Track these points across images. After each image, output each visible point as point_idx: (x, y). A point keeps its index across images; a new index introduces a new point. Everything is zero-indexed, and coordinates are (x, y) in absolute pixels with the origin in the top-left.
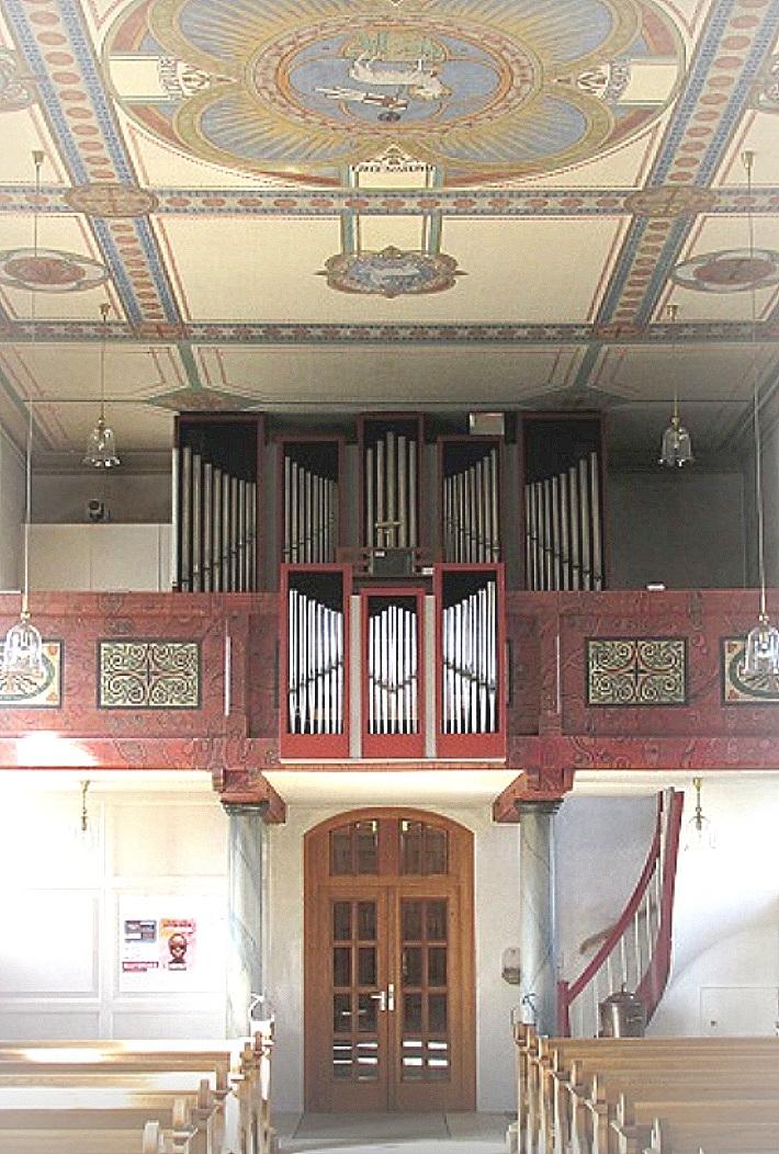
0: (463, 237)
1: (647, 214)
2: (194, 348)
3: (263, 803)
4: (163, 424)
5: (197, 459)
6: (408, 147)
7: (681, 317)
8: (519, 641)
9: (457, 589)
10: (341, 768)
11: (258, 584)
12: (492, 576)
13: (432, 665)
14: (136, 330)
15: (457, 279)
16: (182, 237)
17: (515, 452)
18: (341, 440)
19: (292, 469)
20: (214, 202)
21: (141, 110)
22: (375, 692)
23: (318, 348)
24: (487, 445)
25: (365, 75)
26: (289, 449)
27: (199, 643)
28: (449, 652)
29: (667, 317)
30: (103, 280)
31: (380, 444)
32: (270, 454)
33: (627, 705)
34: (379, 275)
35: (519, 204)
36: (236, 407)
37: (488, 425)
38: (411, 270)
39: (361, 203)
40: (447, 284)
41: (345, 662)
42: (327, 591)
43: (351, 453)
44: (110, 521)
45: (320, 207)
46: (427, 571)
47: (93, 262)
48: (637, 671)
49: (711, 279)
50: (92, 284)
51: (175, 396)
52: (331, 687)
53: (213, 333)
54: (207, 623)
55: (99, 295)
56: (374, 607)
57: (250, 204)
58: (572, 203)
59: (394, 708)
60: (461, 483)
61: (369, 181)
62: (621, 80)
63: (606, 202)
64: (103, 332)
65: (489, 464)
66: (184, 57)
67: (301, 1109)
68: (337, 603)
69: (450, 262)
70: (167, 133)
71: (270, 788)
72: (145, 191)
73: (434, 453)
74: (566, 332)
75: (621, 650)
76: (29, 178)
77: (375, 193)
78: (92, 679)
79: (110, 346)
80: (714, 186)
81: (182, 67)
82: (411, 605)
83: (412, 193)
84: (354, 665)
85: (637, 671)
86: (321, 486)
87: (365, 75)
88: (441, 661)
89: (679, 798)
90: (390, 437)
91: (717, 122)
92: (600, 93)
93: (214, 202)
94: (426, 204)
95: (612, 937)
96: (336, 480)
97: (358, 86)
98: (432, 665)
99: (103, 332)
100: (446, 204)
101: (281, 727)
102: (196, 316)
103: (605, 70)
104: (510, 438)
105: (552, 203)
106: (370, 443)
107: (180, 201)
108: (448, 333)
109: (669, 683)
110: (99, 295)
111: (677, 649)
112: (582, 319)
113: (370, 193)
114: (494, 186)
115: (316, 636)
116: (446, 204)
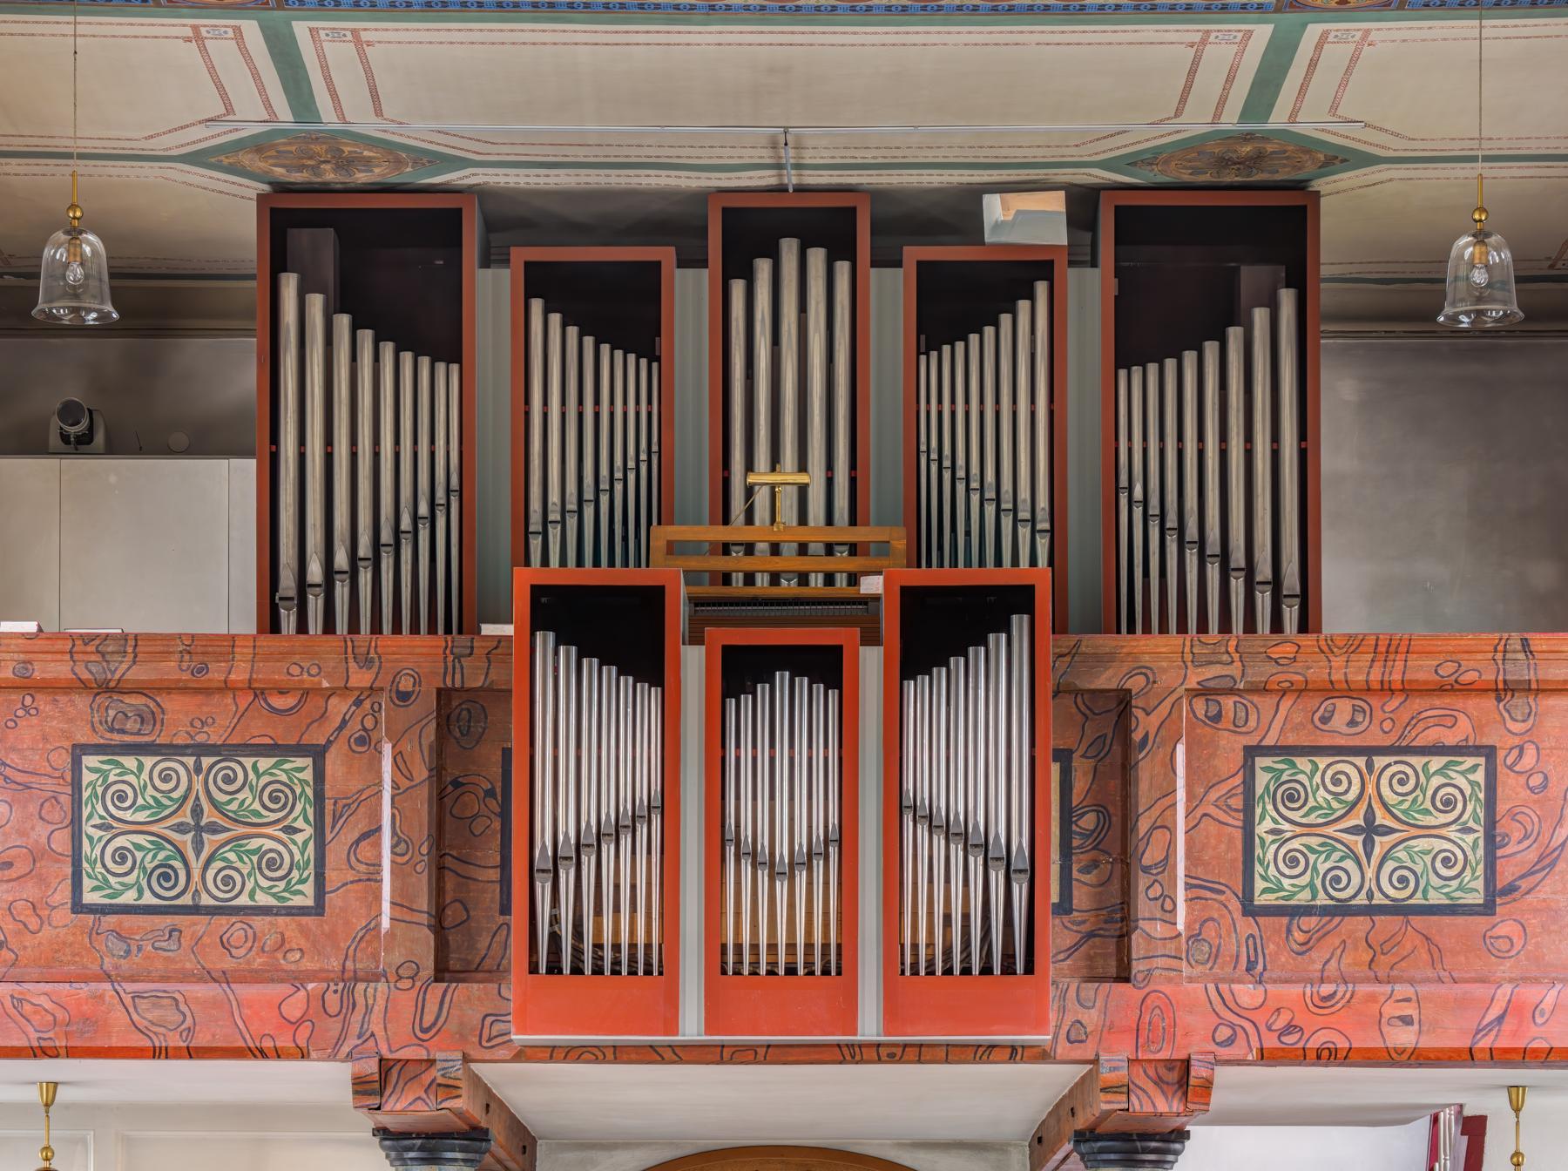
3: (474, 1136)
5: (316, 302)
8: (1096, 749)
17: (1089, 294)
18: (665, 255)
19: (552, 333)
24: (1020, 275)
27: (318, 754)
28: (922, 781)
31: (763, 267)
32: (491, 293)
33: (1343, 910)
36: (408, 175)
37: (1022, 220)
43: (689, 294)
46: (872, 585)
51: (258, 145)
52: (629, 867)
71: (491, 1102)
73: (892, 294)
75: (1326, 782)
78: (61, 841)
82: (826, 667)
85: (1370, 830)
86: (620, 370)
89: (1474, 1128)
90: (789, 248)
106: (737, 266)
109: (1437, 856)
111: (1468, 776)
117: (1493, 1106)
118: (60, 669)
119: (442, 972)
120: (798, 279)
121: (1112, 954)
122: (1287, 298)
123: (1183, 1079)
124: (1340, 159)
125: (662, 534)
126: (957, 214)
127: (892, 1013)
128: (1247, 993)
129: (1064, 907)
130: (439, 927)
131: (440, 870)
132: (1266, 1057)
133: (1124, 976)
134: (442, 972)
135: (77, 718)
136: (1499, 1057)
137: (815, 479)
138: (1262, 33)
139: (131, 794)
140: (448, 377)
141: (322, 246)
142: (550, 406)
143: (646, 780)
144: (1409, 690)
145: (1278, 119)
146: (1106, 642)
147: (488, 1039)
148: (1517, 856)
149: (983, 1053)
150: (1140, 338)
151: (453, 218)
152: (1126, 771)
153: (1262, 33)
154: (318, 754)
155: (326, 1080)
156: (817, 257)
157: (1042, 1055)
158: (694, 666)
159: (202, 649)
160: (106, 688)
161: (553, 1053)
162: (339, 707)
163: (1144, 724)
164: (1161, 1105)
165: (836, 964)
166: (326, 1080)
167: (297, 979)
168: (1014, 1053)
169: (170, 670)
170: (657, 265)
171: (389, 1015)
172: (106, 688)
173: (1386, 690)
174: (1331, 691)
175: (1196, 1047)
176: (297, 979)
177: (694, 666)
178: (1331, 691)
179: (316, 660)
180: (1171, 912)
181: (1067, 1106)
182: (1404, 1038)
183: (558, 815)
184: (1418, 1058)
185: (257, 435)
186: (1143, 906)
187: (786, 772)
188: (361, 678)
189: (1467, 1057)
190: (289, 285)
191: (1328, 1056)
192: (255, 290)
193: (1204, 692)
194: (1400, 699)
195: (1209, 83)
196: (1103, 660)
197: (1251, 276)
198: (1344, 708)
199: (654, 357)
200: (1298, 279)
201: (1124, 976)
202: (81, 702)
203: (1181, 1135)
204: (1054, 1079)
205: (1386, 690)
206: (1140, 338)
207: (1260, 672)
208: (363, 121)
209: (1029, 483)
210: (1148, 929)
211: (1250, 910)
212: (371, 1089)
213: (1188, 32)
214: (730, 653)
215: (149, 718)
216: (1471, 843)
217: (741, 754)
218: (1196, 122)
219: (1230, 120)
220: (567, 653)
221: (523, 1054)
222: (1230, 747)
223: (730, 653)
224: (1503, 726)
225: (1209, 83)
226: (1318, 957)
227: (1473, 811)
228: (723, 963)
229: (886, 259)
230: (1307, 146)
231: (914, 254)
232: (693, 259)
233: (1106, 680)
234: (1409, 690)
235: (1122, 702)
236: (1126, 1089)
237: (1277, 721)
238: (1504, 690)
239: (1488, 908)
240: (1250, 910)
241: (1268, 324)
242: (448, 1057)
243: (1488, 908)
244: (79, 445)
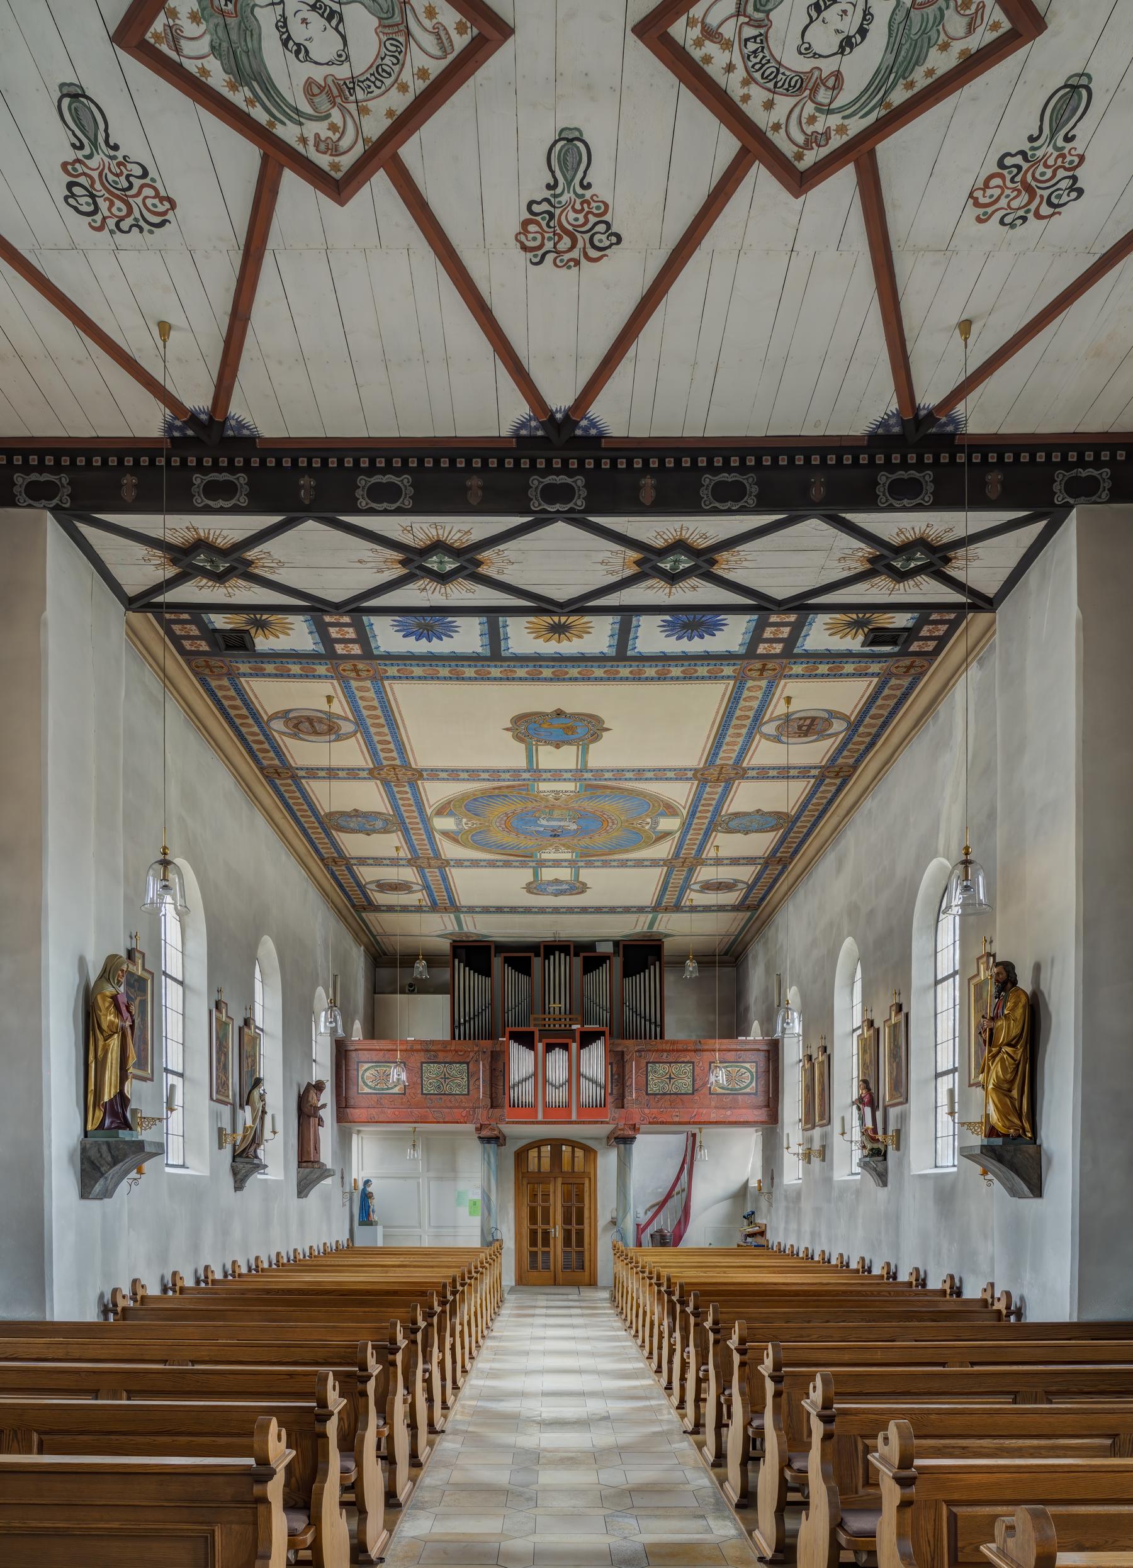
0: (586, 875)
1: (674, 866)
2: (462, 916)
3: (497, 1138)
4: (445, 945)
5: (462, 965)
6: (564, 845)
7: (695, 903)
8: (617, 1063)
9: (587, 1039)
10: (533, 1123)
11: (491, 1036)
12: (603, 1033)
13: (575, 1073)
14: (434, 908)
15: (605, 734)
16: (459, 878)
17: (618, 962)
18: (532, 955)
19: (509, 971)
20: (475, 863)
21: (446, 834)
22: (549, 1088)
23: (522, 916)
24: (602, 959)
25: (544, 822)
26: (507, 960)
27: (468, 1064)
28: (583, 1070)
29: (688, 903)
30: (355, 733)
31: (552, 957)
32: (497, 962)
33: (665, 1094)
34: (550, 889)
35: (615, 864)
36: (480, 939)
37: (606, 948)
38: (565, 887)
39: (542, 864)
40: (582, 892)
41: (535, 1074)
42: (526, 1040)
43: (537, 962)
44: (419, 992)
45: (523, 865)
46: (574, 1027)
47: (346, 719)
48: (670, 1078)
49: (708, 889)
50: (416, 891)
51: (451, 934)
52: (529, 1086)
53: (471, 910)
54: (472, 1054)
55: (419, 895)
56: (549, 1048)
57: (492, 864)
58: (639, 863)
59: (557, 1096)
60: (594, 975)
61: (545, 856)
62: (657, 823)
63: (654, 863)
64: (419, 909)
65: (606, 967)
66: (466, 816)
67: (513, 1284)
68: (531, 1046)
69: (584, 884)
70: (456, 841)
71: (500, 1132)
72: (415, 770)
73: (578, 962)
74: (641, 910)
75: (662, 1069)
76: (394, 854)
77: (549, 860)
78: (419, 1081)
79: (423, 915)
80: (745, 765)
81: (464, 820)
82: (565, 1047)
83: (566, 861)
84: (539, 1075)
85: (670, 1078)
86: (524, 979)
87: (544, 822)
88: (579, 1075)
89: (694, 1135)
90: (557, 953)
91: (749, 721)
92: (647, 827)
93: (475, 863)
94: (572, 864)
95: (662, 1204)
96: (530, 975)
97: (541, 826)
98: (575, 1073)
99: (419, 909)
100: (581, 864)
101: (507, 1104)
102: (463, 904)
103: (649, 820)
104: (616, 952)
105: (629, 863)
106: (547, 957)
107: (459, 863)
108: (584, 910)
109: (684, 1083)
110: (419, 895)
111: (689, 1067)
112: (648, 904)
113: (545, 860)
114: (603, 858)
115: (521, 1062)
116: (581, 864)
117: (696, 1131)
118: (419, 1047)
119: (492, 1107)
120: (559, 958)
121: (620, 1102)
122: (657, 963)
123: (635, 1128)
124: (667, 936)
125: (532, 1017)
126: (590, 946)
127: (579, 1114)
128: (647, 1111)
129: (611, 1094)
130: (491, 1098)
131: (491, 1087)
132: (650, 1123)
133: (623, 1107)
134: (492, 1107)
135: (421, 1057)
136: (695, 1123)
137: (562, 1005)
138: (650, 916)
139: (432, 1071)
140: (488, 980)
141: (463, 953)
142: (509, 988)
143: (531, 1069)
144: (678, 1051)
145: (655, 929)
146: (620, 1041)
147: (501, 1120)
148: (698, 1083)
149: (596, 1123)
150: (628, 972)
151: (489, 947)
152: (623, 1066)
153: (650, 916)
154: (468, 1064)
155: (470, 1127)
156: (563, 955)
157: (607, 1123)
158: (540, 1046)
159: (444, 1042)
160: (427, 1051)
161: (513, 1123)
162: (472, 1054)
163: (627, 1058)
164: (631, 1133)
165: (568, 1106)
166: (470, 1127)
167: (465, 1108)
168: (602, 1122)
169: (440, 1047)
170: (530, 957)
171: (482, 1115)
172: (427, 1051)
173: (673, 1051)
174: (663, 1051)
175: (637, 1121)
176: (465, 1108)
177: (540, 1046)
178: (663, 1051)
179: (468, 1045)
180: (632, 1095)
181: (613, 1132)
182: (677, 1119)
183: (515, 1076)
184: (679, 1123)
185: (447, 988)
186: (627, 1094)
187: (557, 1065)
188: (476, 1049)
189: (689, 1123)
190: (456, 961)
191: (662, 1123)
192: (450, 958)
193: (638, 1051)
194: (678, 1051)
195: (640, 924)
196: (618, 1045)
197: (650, 959)
198: (665, 1054)
199: (530, 975)
200: (659, 960)
201: (623, 1107)
202: (422, 1053)
203: (633, 1139)
204: (610, 1127)
205: (673, 1051)
206: (628, 972)
207: (649, 1047)
208: (472, 930)
209: (605, 1002)
210: (628, 1098)
211: (647, 1094)
212: (479, 1129)
213: (636, 915)
214: (547, 1045)
215: (435, 1056)
216: (689, 1081)
217: (549, 1064)
218: (638, 929)
219: (645, 929)
220: (516, 1045)
221: (508, 1123)
222: (644, 1062)
223: (547, 1045)
224: (696, 1058)
225: (640, 924)
226: (659, 1105)
227: (690, 1075)
228: (545, 1105)
229: (576, 955)
230: (661, 934)
231: (582, 954)
232: (537, 955)
233: (619, 1049)
234: (678, 1051)
235: (623, 1052)
236: (623, 1130)
237: (652, 1057)
238: (696, 1051)
239: (693, 1094)
240: (647, 1094)
241: (653, 971)
242: (493, 1123)
243: (693, 1094)
244: (412, 992)
